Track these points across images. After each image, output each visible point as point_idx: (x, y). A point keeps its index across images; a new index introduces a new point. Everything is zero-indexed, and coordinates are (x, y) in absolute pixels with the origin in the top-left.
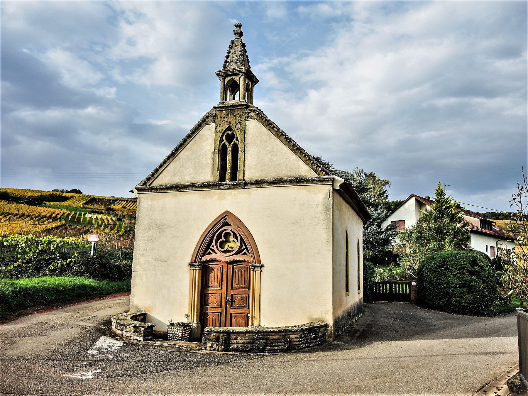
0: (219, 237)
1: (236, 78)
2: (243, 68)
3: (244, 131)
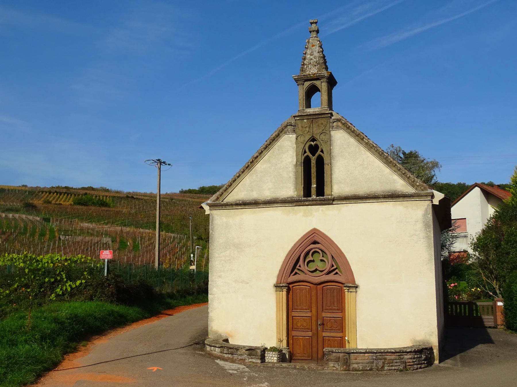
1: (317, 83)
2: (325, 73)
3: (329, 141)
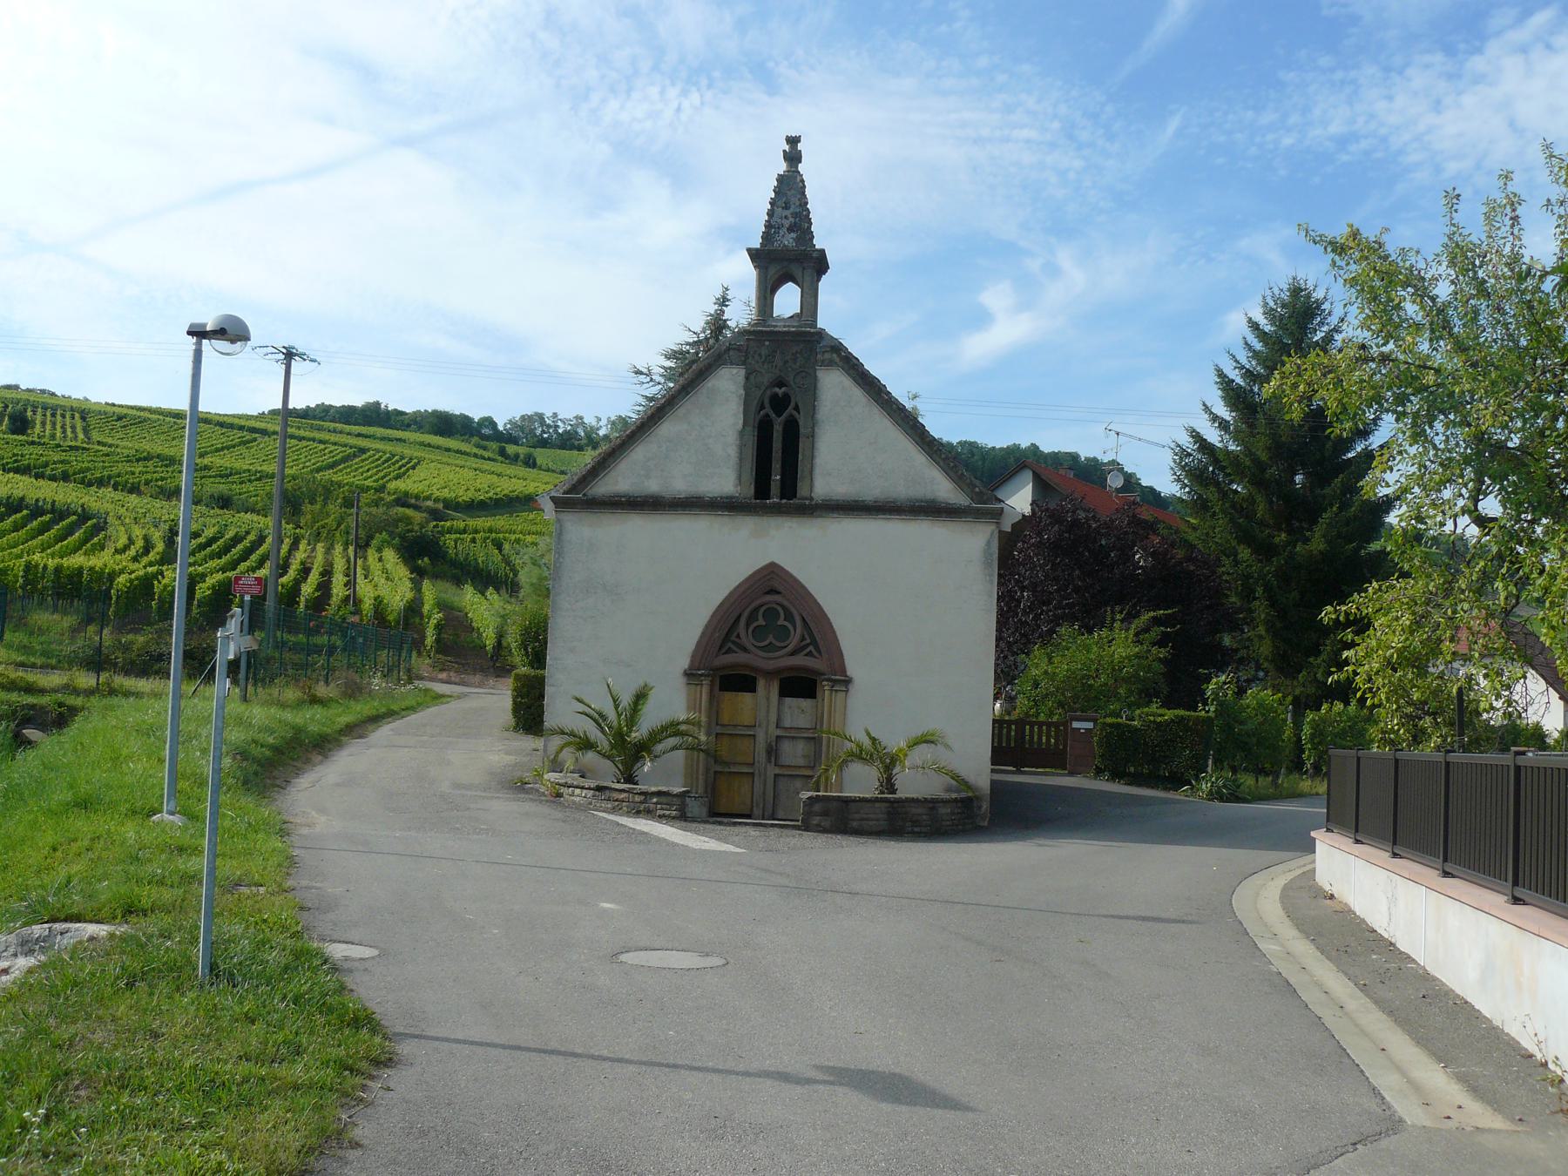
0: (752, 617)
